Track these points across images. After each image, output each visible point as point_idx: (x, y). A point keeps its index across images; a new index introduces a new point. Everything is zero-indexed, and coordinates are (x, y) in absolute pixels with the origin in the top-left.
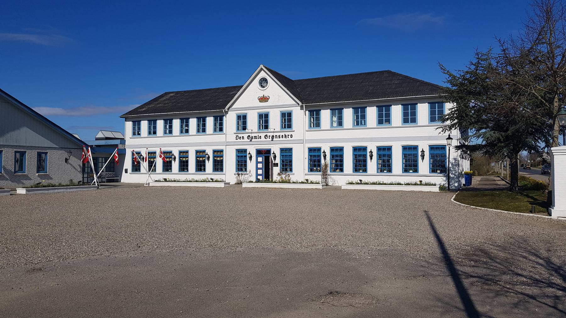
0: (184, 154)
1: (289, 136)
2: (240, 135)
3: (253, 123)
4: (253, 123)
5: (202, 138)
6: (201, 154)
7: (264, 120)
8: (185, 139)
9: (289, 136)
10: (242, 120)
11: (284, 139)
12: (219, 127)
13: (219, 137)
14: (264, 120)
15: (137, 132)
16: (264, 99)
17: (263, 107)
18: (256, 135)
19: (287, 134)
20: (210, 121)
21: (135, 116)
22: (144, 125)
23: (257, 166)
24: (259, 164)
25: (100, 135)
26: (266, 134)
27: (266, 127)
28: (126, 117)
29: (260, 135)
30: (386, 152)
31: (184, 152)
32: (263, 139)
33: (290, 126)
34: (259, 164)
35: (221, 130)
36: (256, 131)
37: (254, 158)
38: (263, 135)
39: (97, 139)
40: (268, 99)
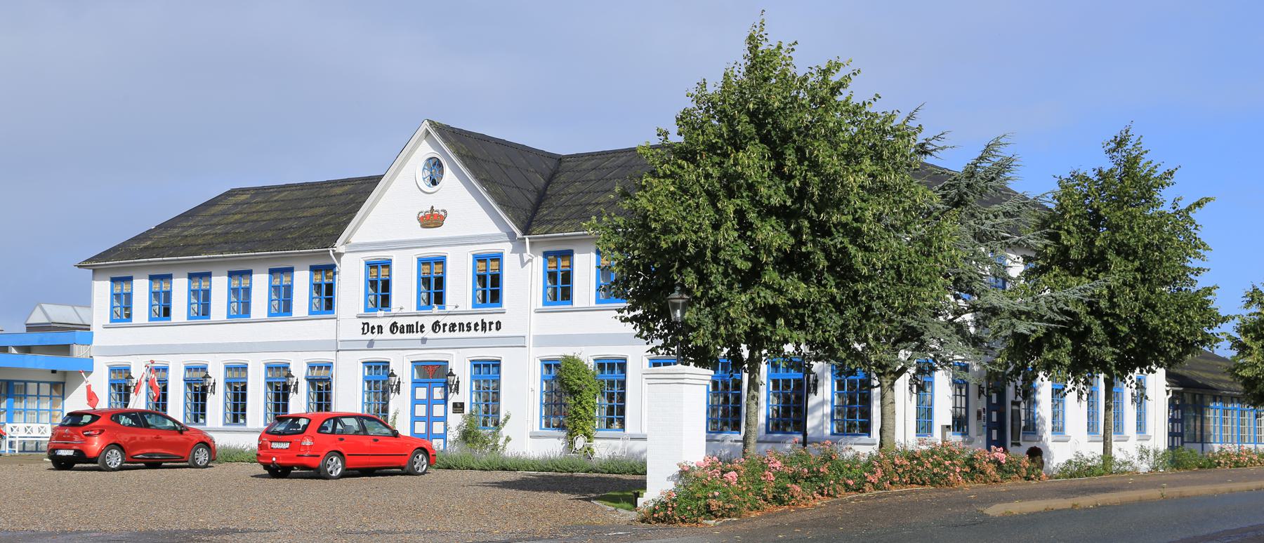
0: (237, 373)
1: (494, 326)
2: (372, 322)
3: (405, 291)
4: (405, 291)
5: (282, 330)
6: (237, 373)
7: (433, 288)
8: (240, 332)
9: (494, 326)
10: (380, 291)
11: (480, 333)
12: (326, 298)
13: (322, 329)
14: (433, 288)
15: (123, 310)
16: (432, 219)
17: (432, 241)
18: (412, 321)
19: (487, 319)
20: (302, 281)
21: (117, 262)
22: (141, 288)
23: (413, 393)
24: (424, 414)
25: (37, 318)
26: (434, 319)
27: (440, 299)
28: (100, 264)
29: (421, 321)
30: (323, 373)
31: (237, 368)
32: (428, 332)
33: (496, 297)
34: (424, 414)
35: (330, 305)
36: (414, 310)
37: (406, 387)
38: (428, 322)
39: (31, 328)
40: (443, 218)
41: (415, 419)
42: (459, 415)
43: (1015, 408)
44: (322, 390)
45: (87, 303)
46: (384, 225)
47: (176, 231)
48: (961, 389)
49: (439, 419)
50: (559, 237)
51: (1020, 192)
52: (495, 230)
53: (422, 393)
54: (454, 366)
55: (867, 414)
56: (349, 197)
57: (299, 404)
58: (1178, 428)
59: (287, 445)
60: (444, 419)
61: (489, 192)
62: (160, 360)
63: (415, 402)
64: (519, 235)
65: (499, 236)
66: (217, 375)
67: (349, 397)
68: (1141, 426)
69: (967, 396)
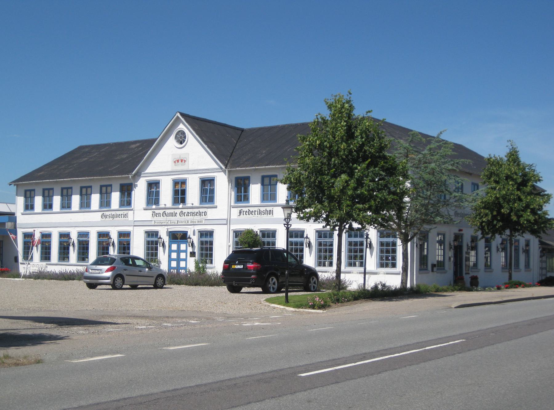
0: (46, 236)
1: (203, 214)
7: (180, 195)
14: (180, 195)
15: (29, 207)
41: (170, 260)
42: (193, 258)
43: (467, 256)
44: (125, 247)
45: (14, 203)
46: (163, 163)
47: (55, 167)
48: (441, 246)
49: (183, 260)
50: (242, 171)
51: (381, 119)
52: (217, 167)
53: (174, 247)
54: (190, 233)
55: (394, 258)
56: (143, 150)
57: (113, 252)
58: (544, 265)
59: (242, 267)
60: (185, 260)
61: (208, 147)
62: (46, 230)
63: (170, 251)
64: (224, 167)
65: (217, 169)
66: (74, 237)
67: (138, 249)
68: (527, 265)
69: (444, 250)
